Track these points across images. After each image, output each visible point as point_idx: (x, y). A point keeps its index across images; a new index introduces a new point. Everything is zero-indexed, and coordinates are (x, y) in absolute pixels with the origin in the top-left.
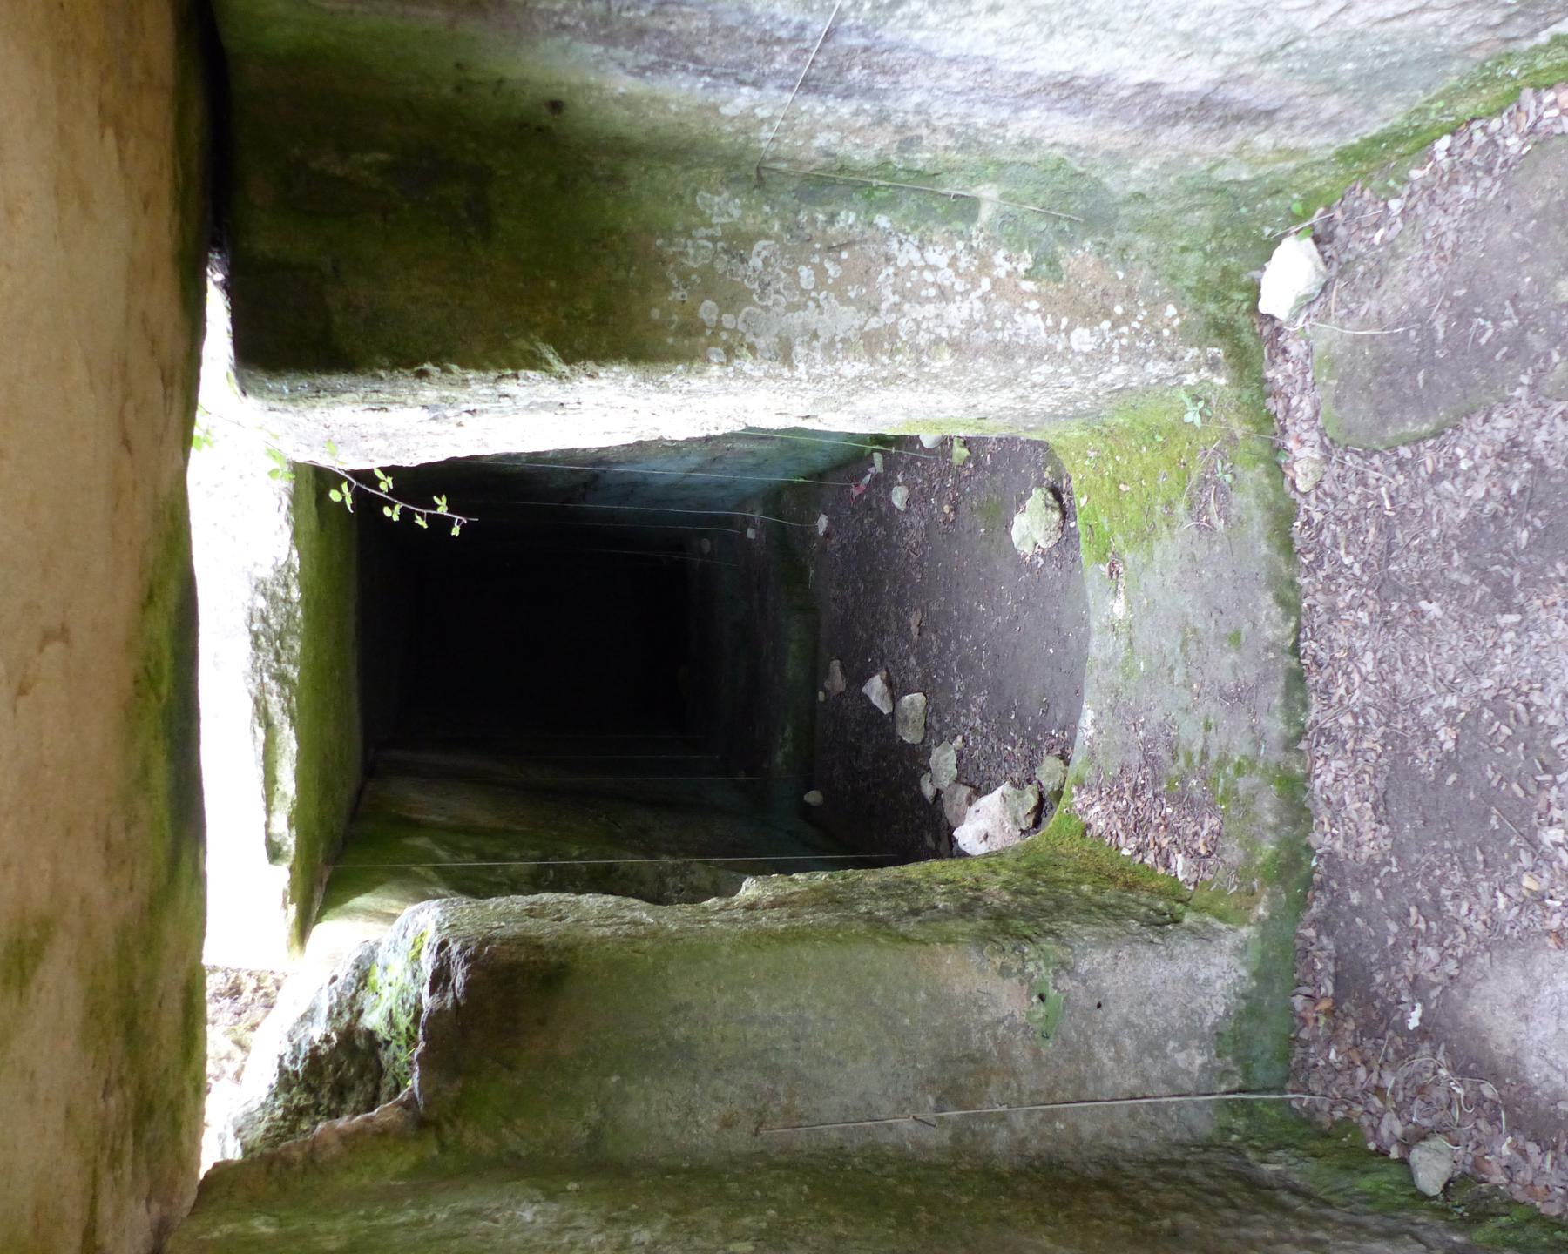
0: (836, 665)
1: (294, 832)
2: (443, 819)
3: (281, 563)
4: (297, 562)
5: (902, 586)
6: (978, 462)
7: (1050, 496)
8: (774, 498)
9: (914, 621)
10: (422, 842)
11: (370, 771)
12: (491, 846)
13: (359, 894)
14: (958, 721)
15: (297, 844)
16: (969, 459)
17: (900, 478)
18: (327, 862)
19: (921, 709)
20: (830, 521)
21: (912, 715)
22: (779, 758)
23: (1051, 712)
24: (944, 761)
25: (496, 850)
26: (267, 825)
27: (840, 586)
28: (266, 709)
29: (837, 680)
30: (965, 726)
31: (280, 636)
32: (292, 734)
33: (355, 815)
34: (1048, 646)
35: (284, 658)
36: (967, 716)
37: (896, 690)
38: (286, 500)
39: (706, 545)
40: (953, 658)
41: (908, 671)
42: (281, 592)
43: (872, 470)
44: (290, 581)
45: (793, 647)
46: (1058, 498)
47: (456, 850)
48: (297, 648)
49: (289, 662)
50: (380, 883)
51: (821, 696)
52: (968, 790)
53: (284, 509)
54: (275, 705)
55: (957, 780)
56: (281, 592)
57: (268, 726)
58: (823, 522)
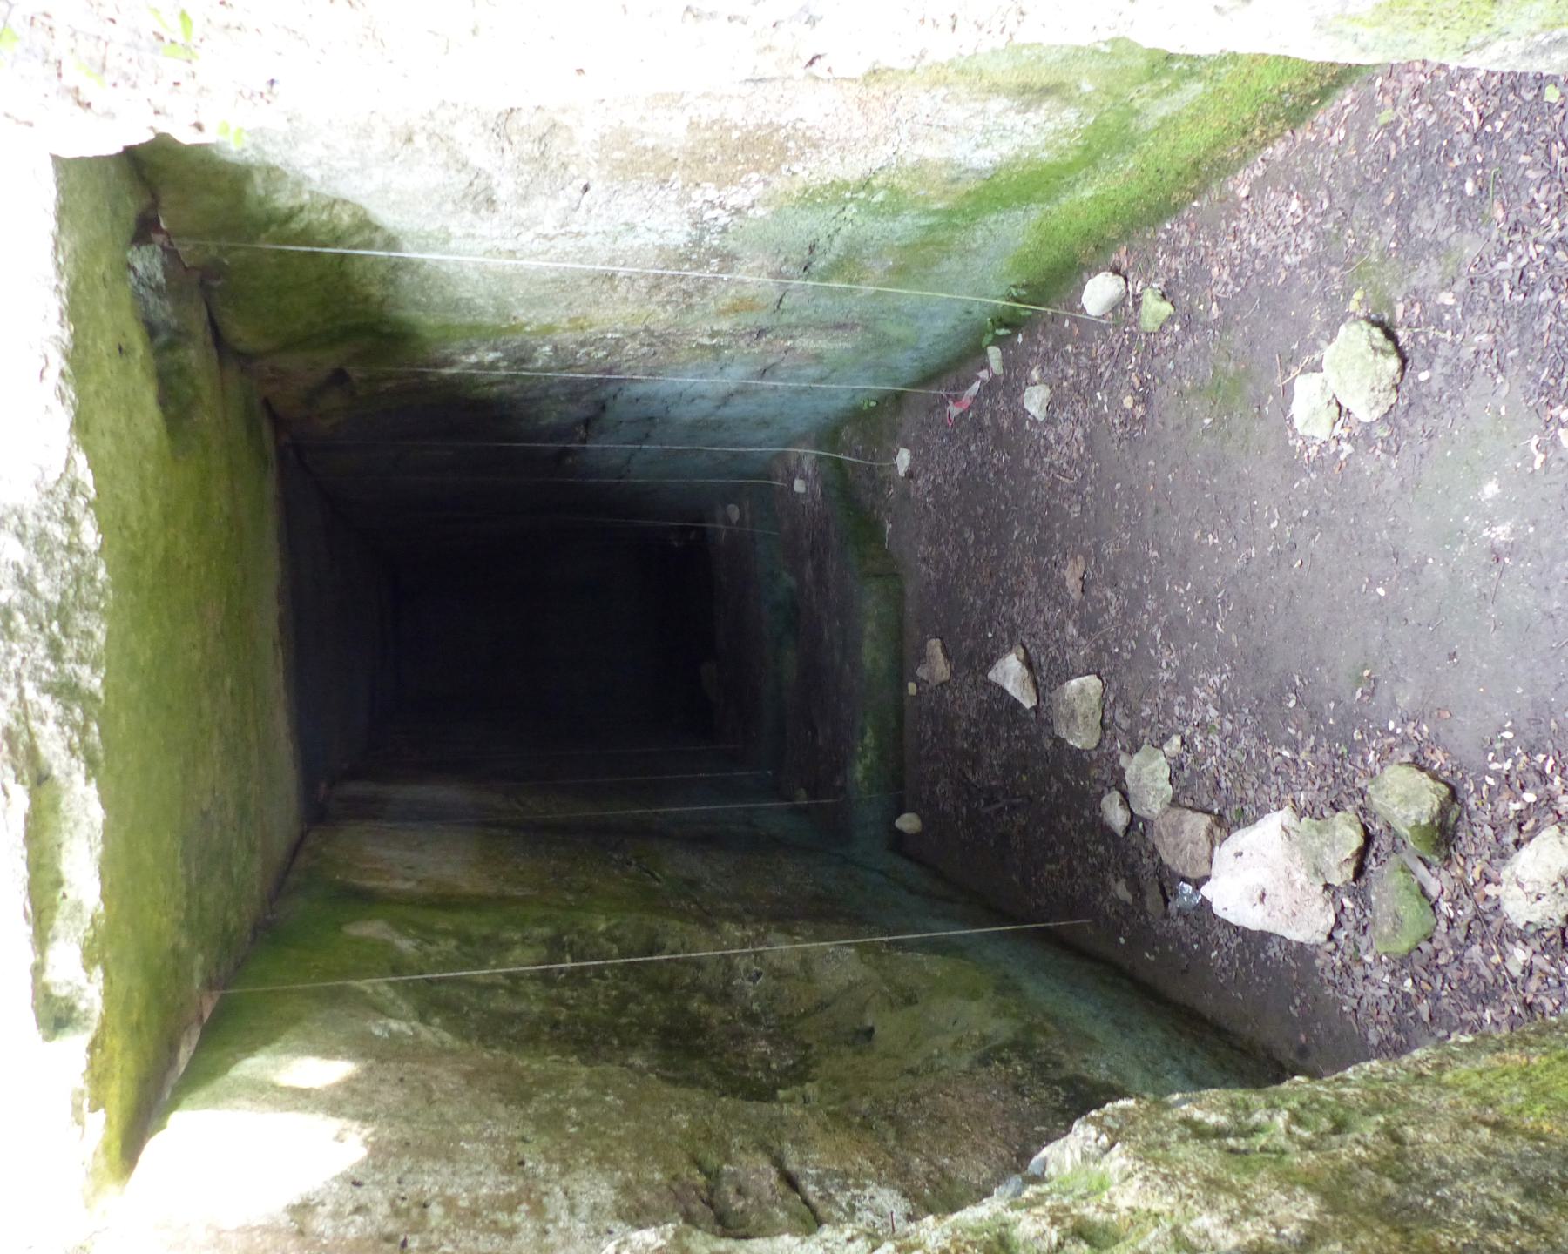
0: (935, 646)
1: (98, 972)
2: (408, 885)
3: (52, 477)
4: (86, 477)
5: (1045, 527)
6: (1189, 320)
7: (1377, 333)
8: (829, 434)
9: (1072, 576)
10: (372, 929)
11: (318, 815)
12: (480, 925)
13: (251, 1050)
14: (1169, 715)
15: (107, 995)
16: (1171, 319)
17: (1035, 374)
18: (210, 984)
19: (1096, 699)
20: (914, 455)
21: (1081, 708)
22: (859, 772)
23: (1384, 694)
24: (1150, 775)
25: (486, 931)
26: (38, 969)
27: (933, 541)
28: (32, 753)
29: (937, 666)
30: (1185, 721)
31: (62, 613)
32: (92, 791)
33: (281, 886)
34: (1373, 583)
35: (70, 653)
36: (1188, 706)
37: (1045, 676)
38: (57, 363)
39: (734, 512)
40: (1154, 620)
41: (1062, 646)
42: (59, 532)
43: (984, 374)
44: (77, 512)
45: (871, 627)
46: (1390, 335)
47: (427, 934)
48: (100, 636)
49: (81, 660)
50: (294, 1020)
51: (912, 688)
52: (1204, 821)
53: (53, 375)
54: (53, 744)
55: (1175, 802)
56: (59, 532)
57: (40, 779)
58: (903, 459)
